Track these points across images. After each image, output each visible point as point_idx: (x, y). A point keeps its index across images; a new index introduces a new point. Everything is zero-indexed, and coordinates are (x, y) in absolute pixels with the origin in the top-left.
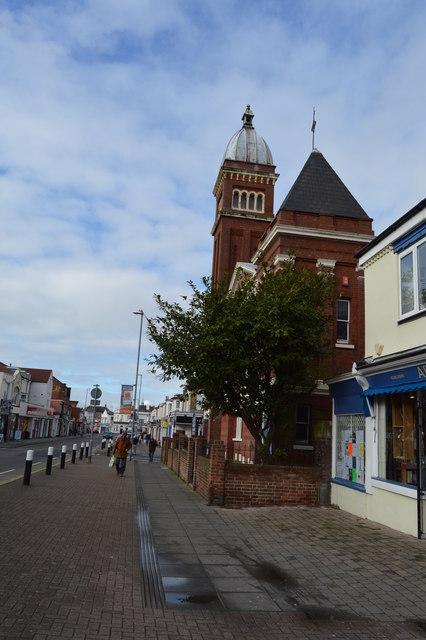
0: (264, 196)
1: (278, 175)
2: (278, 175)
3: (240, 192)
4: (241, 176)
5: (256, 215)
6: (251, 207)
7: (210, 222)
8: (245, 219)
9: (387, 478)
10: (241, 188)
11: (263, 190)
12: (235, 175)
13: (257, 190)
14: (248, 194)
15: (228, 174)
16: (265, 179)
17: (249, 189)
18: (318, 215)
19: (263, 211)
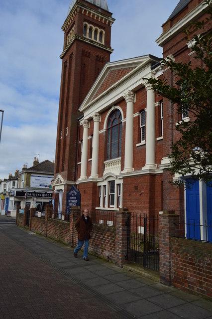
0: (104, 32)
1: (113, 50)
2: (113, 50)
3: (89, 26)
4: (90, 13)
5: (100, 45)
6: (96, 38)
7: (60, 50)
8: (92, 45)
9: (134, 118)
10: (90, 22)
11: (104, 28)
12: (85, 11)
13: (100, 27)
14: (94, 28)
15: (81, 9)
16: (106, 20)
17: (95, 25)
18: (119, 149)
19: (103, 43)
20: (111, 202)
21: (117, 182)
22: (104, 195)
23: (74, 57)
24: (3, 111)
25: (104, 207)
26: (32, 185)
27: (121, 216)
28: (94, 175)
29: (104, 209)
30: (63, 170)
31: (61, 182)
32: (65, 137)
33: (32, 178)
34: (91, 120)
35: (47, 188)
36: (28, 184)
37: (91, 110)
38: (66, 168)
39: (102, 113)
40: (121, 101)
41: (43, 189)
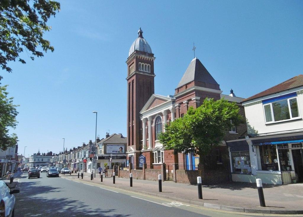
20: (159, 161)
21: (161, 151)
22: (156, 157)
23: (135, 84)
24: (97, 113)
25: (156, 163)
26: (107, 152)
27: (162, 165)
28: (149, 148)
29: (156, 164)
30: (133, 144)
31: (132, 151)
32: (133, 126)
33: (107, 147)
34: (146, 119)
35: (117, 153)
36: (197, 168)
37: (146, 114)
38: (135, 143)
39: (153, 117)
40: (161, 114)
41: (115, 154)
